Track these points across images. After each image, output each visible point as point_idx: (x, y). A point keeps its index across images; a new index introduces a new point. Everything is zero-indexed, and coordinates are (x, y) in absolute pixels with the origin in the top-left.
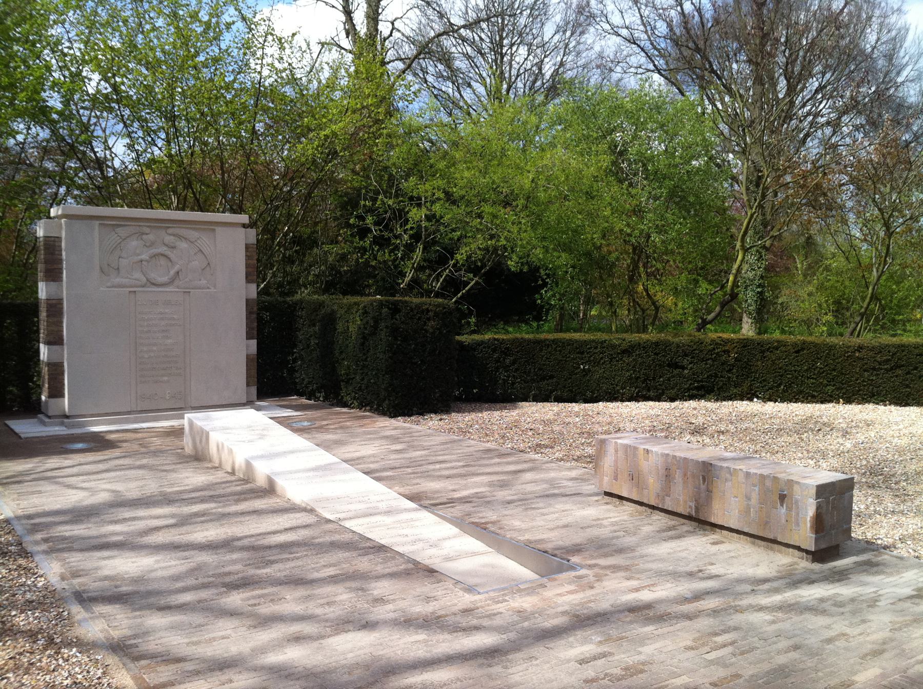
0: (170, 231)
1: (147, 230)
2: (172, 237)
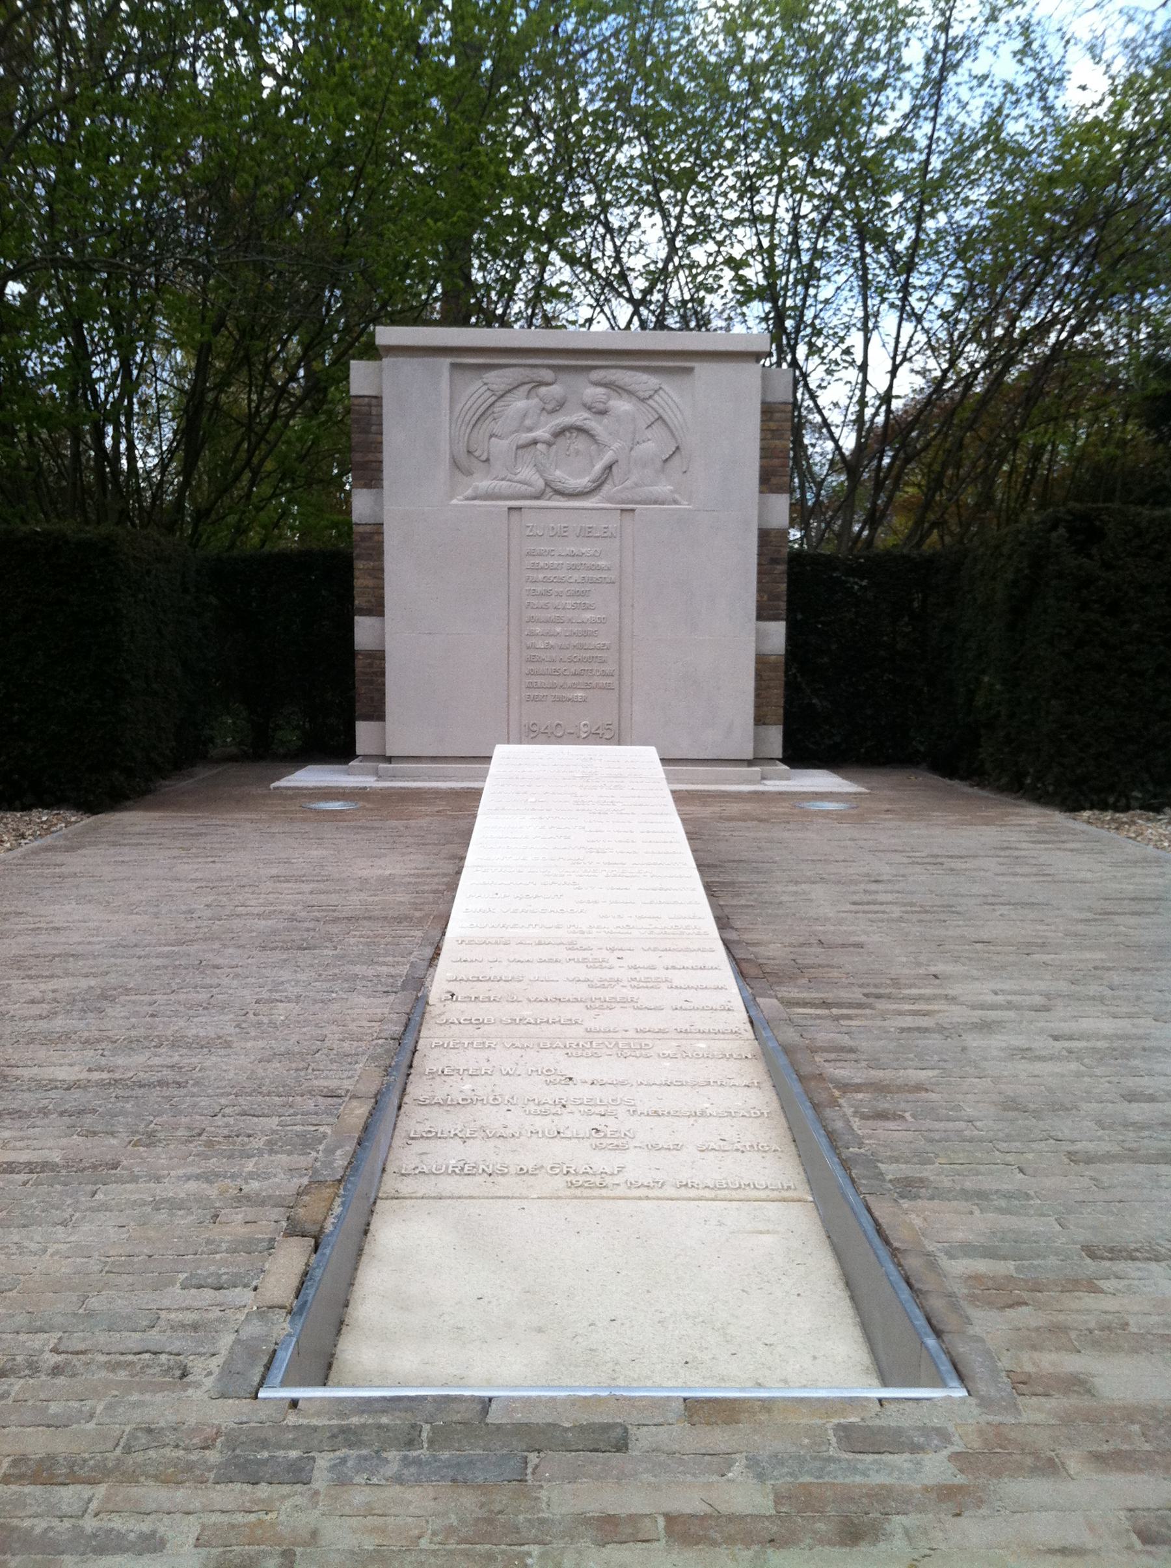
0: (596, 375)
1: (548, 375)
2: (601, 390)
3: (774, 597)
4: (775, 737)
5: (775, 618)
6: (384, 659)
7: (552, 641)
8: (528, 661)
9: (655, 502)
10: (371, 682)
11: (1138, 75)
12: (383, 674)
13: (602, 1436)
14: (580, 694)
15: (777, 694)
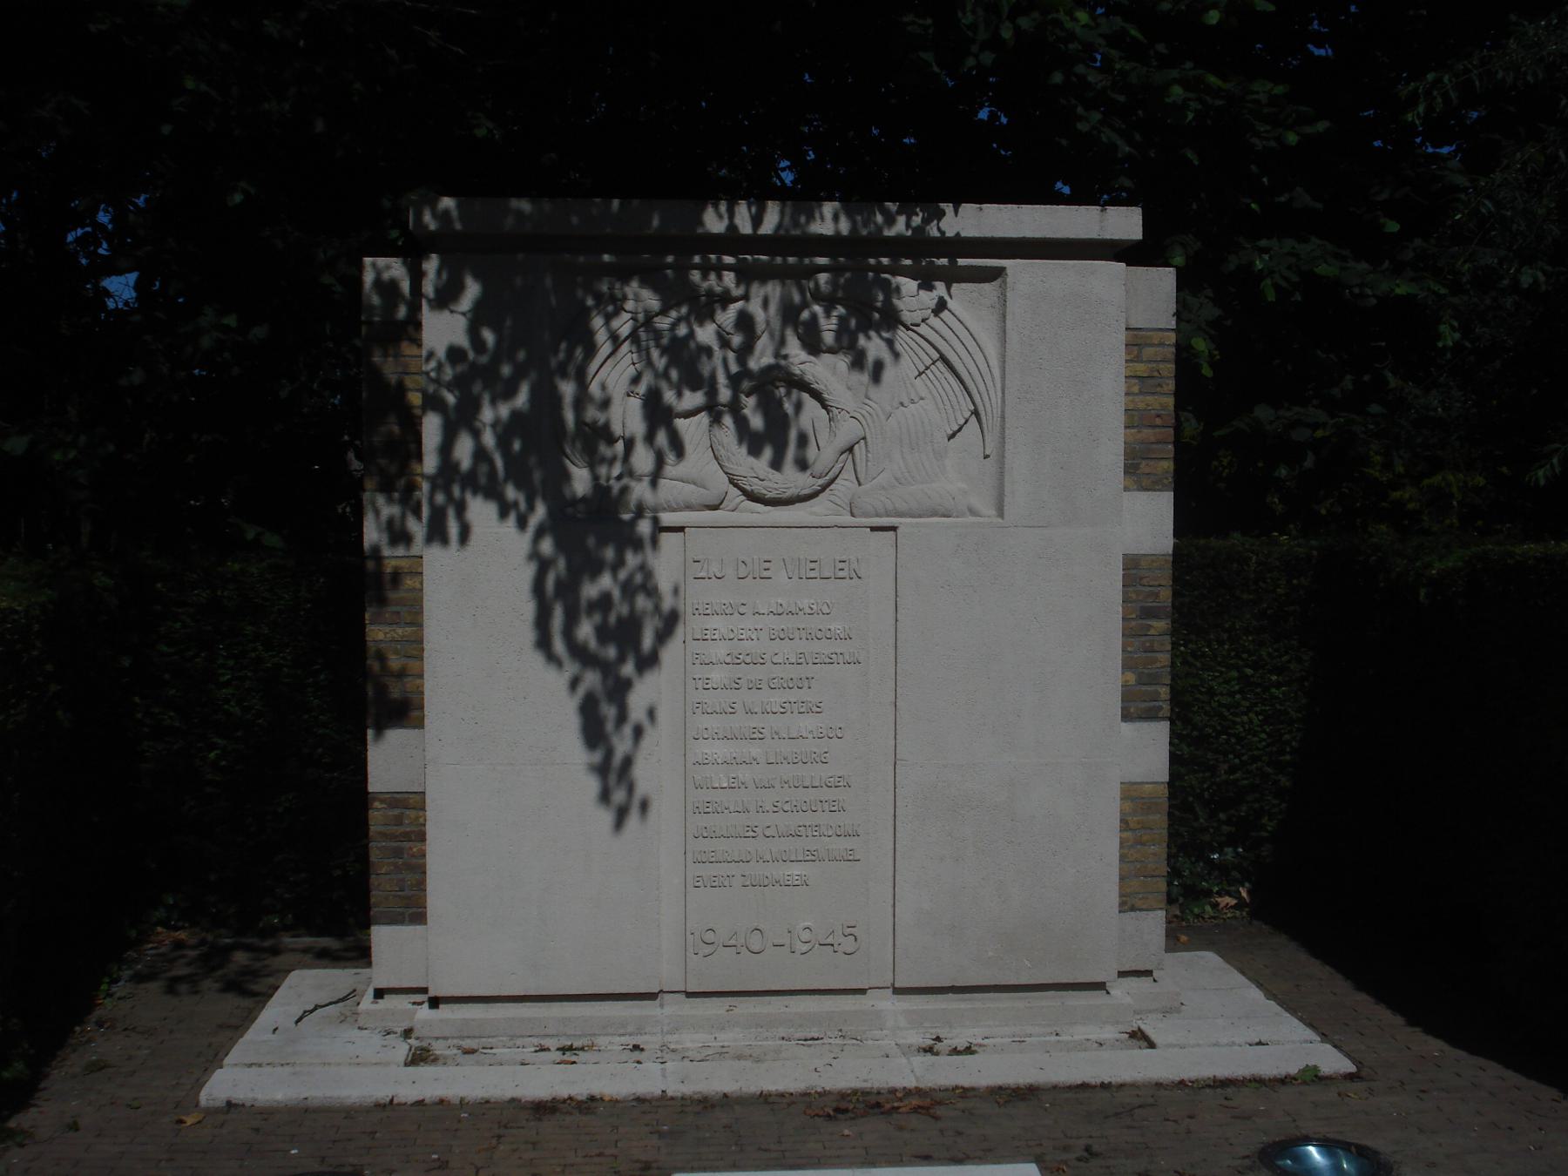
3: (1148, 679)
4: (1154, 923)
5: (1150, 716)
6: (422, 807)
7: (744, 774)
8: (697, 810)
9: (934, 514)
10: (398, 853)
11: (611, 441)
12: (422, 837)
13: (1122, 1086)
14: (796, 870)
15: (1156, 852)
